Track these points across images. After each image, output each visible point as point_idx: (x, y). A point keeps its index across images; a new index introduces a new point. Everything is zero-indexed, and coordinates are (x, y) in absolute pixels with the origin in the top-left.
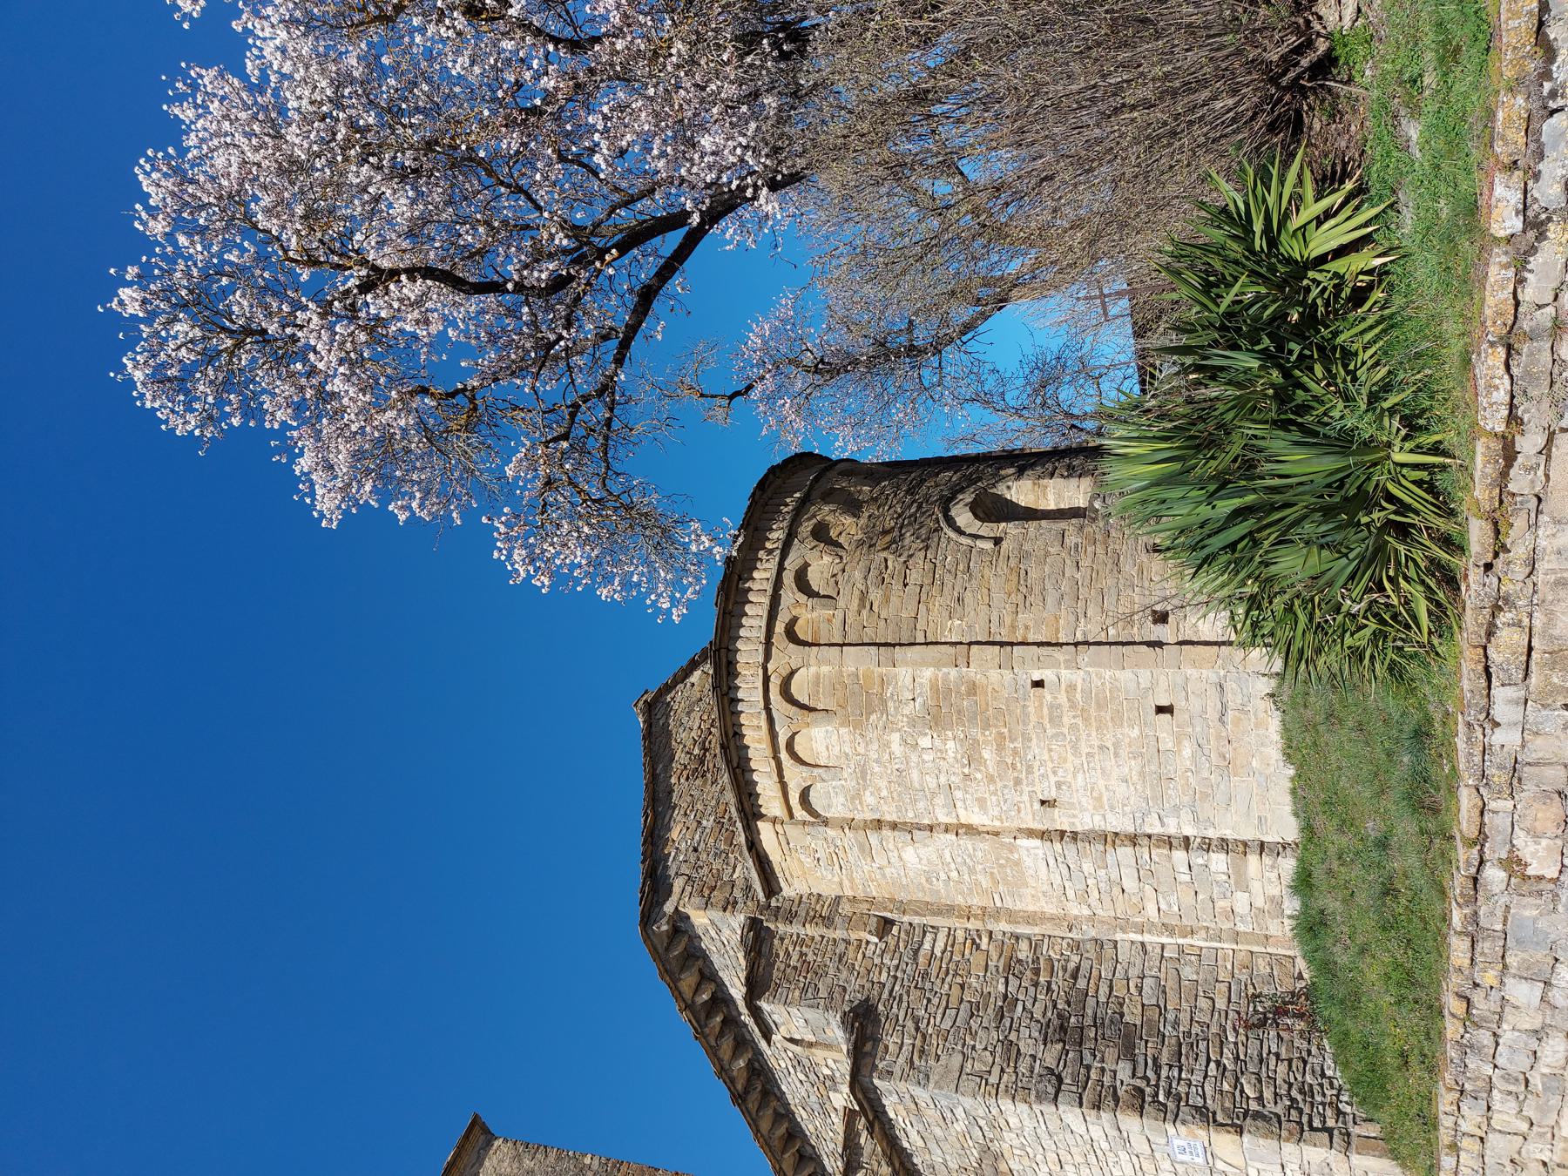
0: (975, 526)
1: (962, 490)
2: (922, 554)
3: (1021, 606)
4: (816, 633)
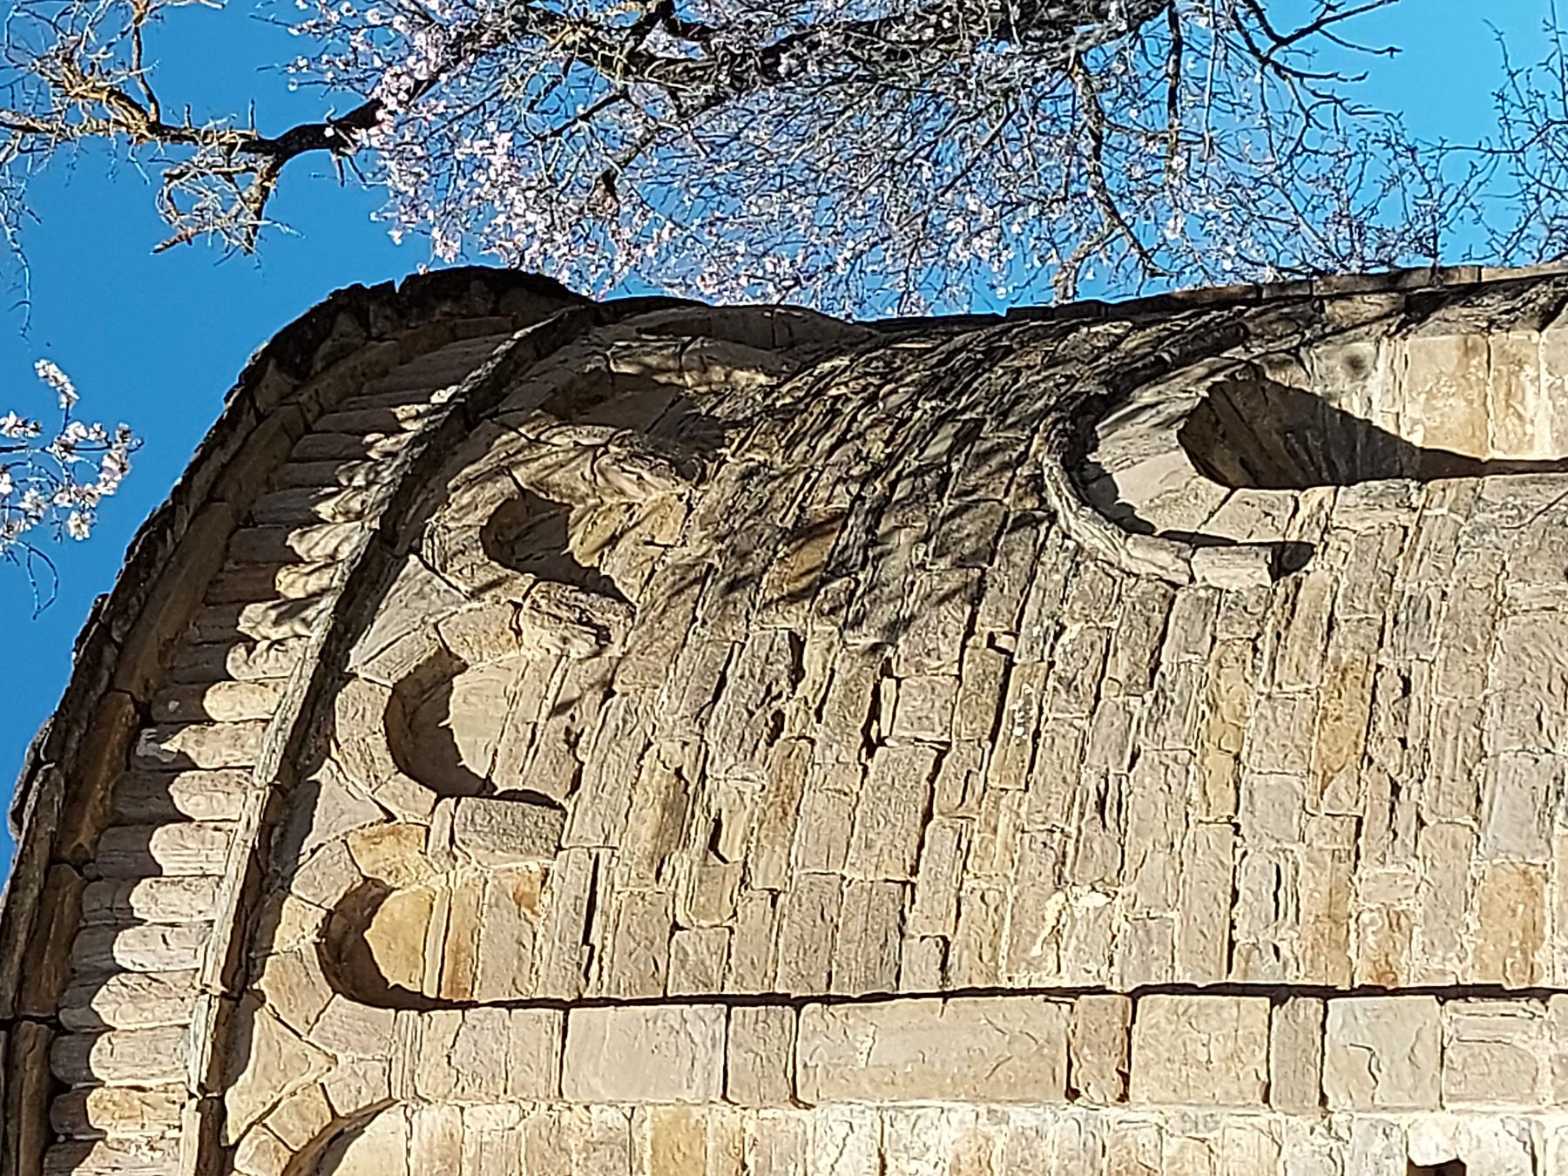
0: (1199, 501)
1: (1157, 372)
2: (954, 616)
3: (1375, 826)
4: (457, 955)
